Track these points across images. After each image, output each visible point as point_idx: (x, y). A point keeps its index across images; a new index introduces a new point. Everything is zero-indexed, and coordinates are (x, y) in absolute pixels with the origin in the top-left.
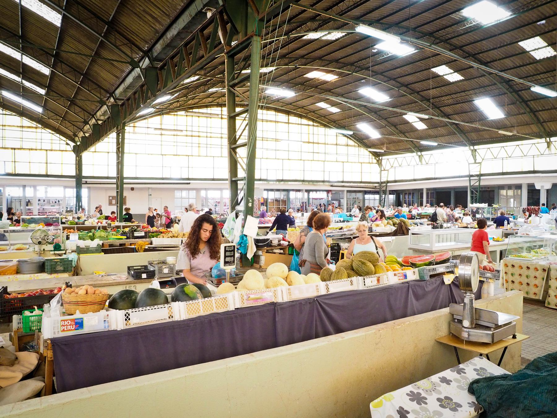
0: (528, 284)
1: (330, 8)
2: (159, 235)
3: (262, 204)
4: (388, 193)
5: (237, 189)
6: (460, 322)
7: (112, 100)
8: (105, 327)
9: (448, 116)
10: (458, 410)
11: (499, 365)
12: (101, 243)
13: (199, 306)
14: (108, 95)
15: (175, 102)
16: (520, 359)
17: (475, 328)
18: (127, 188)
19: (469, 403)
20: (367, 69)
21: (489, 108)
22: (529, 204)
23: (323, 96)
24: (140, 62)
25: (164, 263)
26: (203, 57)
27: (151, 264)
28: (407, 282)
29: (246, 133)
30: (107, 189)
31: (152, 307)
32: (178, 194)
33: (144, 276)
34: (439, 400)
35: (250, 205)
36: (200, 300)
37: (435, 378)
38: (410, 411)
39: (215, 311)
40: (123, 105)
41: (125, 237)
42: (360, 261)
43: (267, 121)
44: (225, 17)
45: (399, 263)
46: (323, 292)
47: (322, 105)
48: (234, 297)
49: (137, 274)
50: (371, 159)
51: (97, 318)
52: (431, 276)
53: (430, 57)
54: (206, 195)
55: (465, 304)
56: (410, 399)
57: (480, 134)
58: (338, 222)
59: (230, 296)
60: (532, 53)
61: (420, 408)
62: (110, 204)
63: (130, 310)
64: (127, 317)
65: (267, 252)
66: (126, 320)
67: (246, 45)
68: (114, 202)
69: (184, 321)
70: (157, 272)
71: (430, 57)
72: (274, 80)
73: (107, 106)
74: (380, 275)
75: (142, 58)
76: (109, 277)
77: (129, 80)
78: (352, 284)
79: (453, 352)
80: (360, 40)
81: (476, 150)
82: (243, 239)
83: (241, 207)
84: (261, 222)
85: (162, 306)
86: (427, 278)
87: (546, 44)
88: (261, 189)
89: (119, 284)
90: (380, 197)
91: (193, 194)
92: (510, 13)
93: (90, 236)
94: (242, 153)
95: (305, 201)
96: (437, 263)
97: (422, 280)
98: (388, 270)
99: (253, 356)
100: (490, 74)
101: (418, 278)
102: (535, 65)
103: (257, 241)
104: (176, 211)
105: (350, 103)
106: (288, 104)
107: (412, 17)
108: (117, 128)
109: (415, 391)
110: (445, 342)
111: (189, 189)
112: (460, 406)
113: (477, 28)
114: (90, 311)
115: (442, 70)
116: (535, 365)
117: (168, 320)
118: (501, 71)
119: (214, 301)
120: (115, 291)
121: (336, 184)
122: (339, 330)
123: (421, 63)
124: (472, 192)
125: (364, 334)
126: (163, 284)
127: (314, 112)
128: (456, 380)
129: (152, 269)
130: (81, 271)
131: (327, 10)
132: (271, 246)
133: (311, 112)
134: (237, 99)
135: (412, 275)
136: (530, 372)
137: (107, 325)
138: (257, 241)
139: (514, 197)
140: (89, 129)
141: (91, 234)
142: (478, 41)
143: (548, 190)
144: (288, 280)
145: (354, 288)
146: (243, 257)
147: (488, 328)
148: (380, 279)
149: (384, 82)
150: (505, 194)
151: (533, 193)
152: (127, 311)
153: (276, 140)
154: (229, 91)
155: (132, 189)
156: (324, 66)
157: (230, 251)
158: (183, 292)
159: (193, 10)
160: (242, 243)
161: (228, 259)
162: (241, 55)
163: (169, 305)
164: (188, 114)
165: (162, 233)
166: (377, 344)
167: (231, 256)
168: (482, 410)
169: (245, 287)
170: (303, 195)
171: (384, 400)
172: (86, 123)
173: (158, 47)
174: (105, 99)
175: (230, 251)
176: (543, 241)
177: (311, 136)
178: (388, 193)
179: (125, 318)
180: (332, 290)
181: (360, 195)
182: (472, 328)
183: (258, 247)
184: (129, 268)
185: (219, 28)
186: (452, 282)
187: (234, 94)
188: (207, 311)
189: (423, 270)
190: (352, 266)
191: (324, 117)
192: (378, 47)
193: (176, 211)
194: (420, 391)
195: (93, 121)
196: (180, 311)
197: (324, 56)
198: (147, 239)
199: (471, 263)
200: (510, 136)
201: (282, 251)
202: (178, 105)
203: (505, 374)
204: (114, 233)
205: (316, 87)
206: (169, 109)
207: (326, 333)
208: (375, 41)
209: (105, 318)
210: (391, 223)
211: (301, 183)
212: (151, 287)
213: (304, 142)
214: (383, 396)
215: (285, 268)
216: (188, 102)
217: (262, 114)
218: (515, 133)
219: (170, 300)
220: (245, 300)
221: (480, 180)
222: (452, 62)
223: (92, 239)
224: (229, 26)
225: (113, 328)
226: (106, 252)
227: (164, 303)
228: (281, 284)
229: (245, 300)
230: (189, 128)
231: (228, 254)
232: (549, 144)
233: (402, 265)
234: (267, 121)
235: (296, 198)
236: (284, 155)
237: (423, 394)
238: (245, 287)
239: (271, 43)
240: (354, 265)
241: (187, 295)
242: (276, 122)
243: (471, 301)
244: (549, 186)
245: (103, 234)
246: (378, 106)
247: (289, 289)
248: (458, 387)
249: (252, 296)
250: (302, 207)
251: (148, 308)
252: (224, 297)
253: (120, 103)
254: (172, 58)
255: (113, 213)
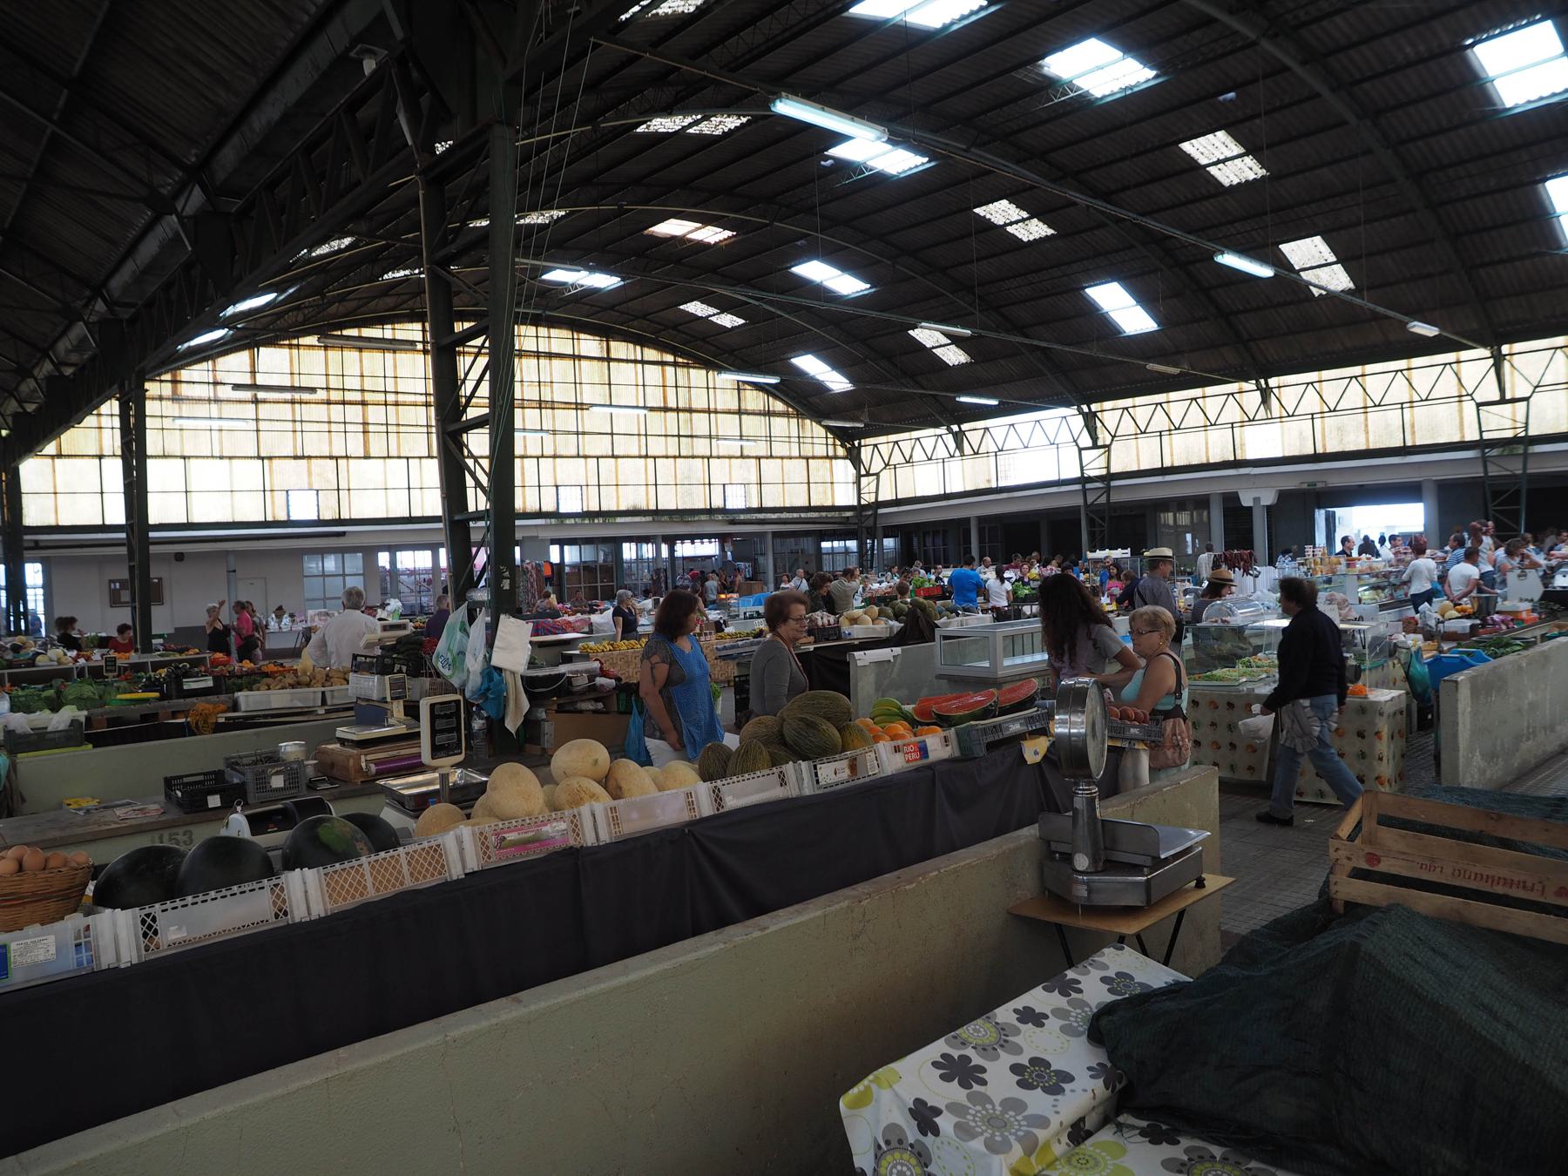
0: (1233, 746)
1: (706, 49)
2: (255, 682)
3: (548, 580)
4: (880, 533)
5: (467, 544)
6: (1068, 858)
7: (100, 306)
8: (80, 964)
9: (1021, 330)
10: (1063, 1090)
11: (1166, 963)
12: (82, 715)
13: (363, 876)
14: (88, 293)
15: (291, 310)
16: (1218, 936)
17: (1104, 871)
18: (163, 557)
19: (1089, 1069)
20: (810, 210)
21: (1121, 307)
22: (1228, 546)
23: (696, 285)
24: (175, 196)
25: (273, 758)
26: (358, 183)
27: (233, 764)
28: (930, 767)
29: (484, 390)
30: (102, 561)
31: (224, 892)
32: (312, 565)
33: (214, 801)
34: (1015, 1069)
35: (506, 585)
36: (364, 859)
37: (1005, 1013)
38: (943, 1108)
39: (409, 884)
40: (132, 321)
41: (156, 694)
42: (801, 719)
43: (550, 356)
44: (415, 74)
45: (905, 717)
46: (706, 809)
47: (696, 308)
48: (460, 842)
49: (190, 797)
50: (831, 448)
51: (52, 938)
52: (991, 746)
53: (967, 180)
54: (393, 562)
55: (1075, 811)
56: (942, 1077)
57: (1092, 372)
58: (751, 617)
59: (449, 841)
60: (1213, 170)
61: (968, 1096)
62: (115, 601)
63: (157, 905)
64: (150, 927)
65: (561, 709)
66: (145, 935)
67: (471, 153)
68: (126, 596)
69: (320, 920)
70: (251, 788)
71: (967, 180)
72: (569, 245)
73: (86, 324)
74: (858, 752)
75: (182, 188)
76: (109, 812)
77: (149, 248)
78: (783, 783)
79: (1047, 942)
80: (788, 136)
81: (1094, 414)
82: (491, 680)
83: (481, 595)
84: (535, 633)
85: (255, 885)
86: (980, 751)
87: (1242, 150)
88: (543, 540)
89: (139, 830)
90: (861, 545)
91: (355, 562)
92: (1154, 73)
93: (47, 698)
94: (478, 443)
95: (662, 566)
96: (1004, 712)
97: (966, 756)
98: (876, 739)
99: (519, 1001)
100: (1119, 221)
101: (957, 754)
102: (1221, 199)
103: (529, 683)
104: (311, 612)
105: (771, 303)
106: (605, 309)
107: (915, 78)
108: (121, 387)
109: (956, 1054)
110: (1033, 915)
111: (342, 551)
112: (1070, 1078)
113: (1084, 103)
114: (33, 922)
115: (1000, 212)
116: (1242, 950)
117: (274, 924)
118: (1143, 215)
119: (403, 860)
120: (113, 854)
121: (742, 517)
122: (757, 907)
123: (941, 198)
124: (1091, 522)
125: (819, 913)
126: (258, 823)
127: (675, 328)
128: (1058, 1013)
129: (236, 781)
130: (23, 800)
131: (694, 55)
132: (571, 693)
133: (666, 327)
134: (456, 300)
135: (938, 745)
136: (1232, 972)
137: (84, 955)
138: (529, 683)
139: (1192, 528)
140: (35, 391)
141: (50, 692)
142: (1083, 140)
143: (1269, 508)
144: (612, 783)
145: (790, 791)
146: (495, 726)
147: (1136, 869)
148: (858, 762)
149: (857, 244)
150: (1171, 522)
151: (1237, 516)
152: (147, 910)
153: (579, 406)
154: (433, 275)
155: (179, 557)
156: (694, 206)
157: (446, 716)
158: (316, 840)
159: (322, 52)
160: (488, 689)
161: (441, 739)
162: (465, 179)
163: (275, 881)
164: (330, 342)
165: (267, 675)
166: (856, 937)
167: (450, 731)
168: (1124, 1083)
169: (491, 813)
170: (658, 551)
171: (874, 1087)
172: (24, 373)
173: (229, 156)
174: (80, 303)
175: (446, 716)
176: (1261, 635)
177: (671, 392)
178: (880, 533)
179: (140, 929)
180: (732, 802)
181: (807, 544)
182: (1096, 873)
183: (532, 698)
184: (169, 783)
185: (400, 103)
186: (1045, 757)
187: (448, 284)
188: (353, 897)
189: (969, 730)
190: (782, 735)
191: (703, 340)
192: (838, 152)
193: (311, 612)
194: (970, 1052)
195: (48, 367)
196: (307, 893)
197: (692, 177)
198: (223, 697)
199: (1083, 704)
200: (1174, 376)
201: (600, 706)
202: (301, 318)
203: (1177, 983)
204: (124, 684)
205: (679, 261)
206: (274, 330)
207: (721, 920)
208: (837, 138)
209: (78, 937)
210: (889, 610)
211: (649, 519)
212: (224, 832)
213: (652, 409)
214: (871, 1077)
215: (601, 753)
216: (326, 311)
217: (527, 337)
218: (1186, 368)
219: (277, 865)
220: (492, 849)
221: (1108, 489)
222: (1024, 190)
223: (55, 707)
224: (425, 100)
225: (107, 960)
226: (99, 741)
227: (259, 878)
228: (593, 796)
229: (492, 849)
230: (335, 382)
231: (440, 724)
232: (1266, 394)
233: (914, 723)
234: (550, 356)
235: (639, 560)
236: (600, 445)
237: (976, 1060)
238: (491, 813)
239: (543, 146)
240: (786, 732)
241: (326, 847)
242: (574, 357)
243: (1091, 802)
244: (1269, 498)
245: (89, 690)
246: (840, 308)
247: (614, 809)
248: (1063, 1029)
249: (511, 836)
250: (656, 582)
251: (213, 894)
252: (433, 843)
253: (125, 314)
254: (272, 185)
255: (122, 629)
